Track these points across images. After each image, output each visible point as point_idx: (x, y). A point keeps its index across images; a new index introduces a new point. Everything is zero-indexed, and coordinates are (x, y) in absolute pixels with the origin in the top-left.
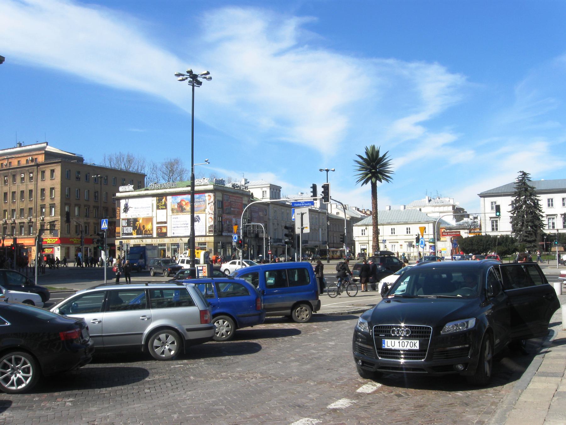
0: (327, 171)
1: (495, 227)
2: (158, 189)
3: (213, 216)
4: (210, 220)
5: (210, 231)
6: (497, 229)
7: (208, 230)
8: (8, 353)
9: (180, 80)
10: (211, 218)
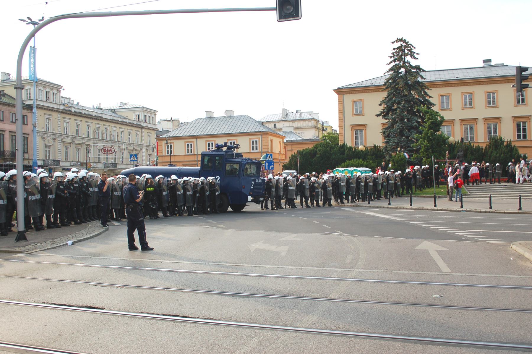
6: (525, 136)
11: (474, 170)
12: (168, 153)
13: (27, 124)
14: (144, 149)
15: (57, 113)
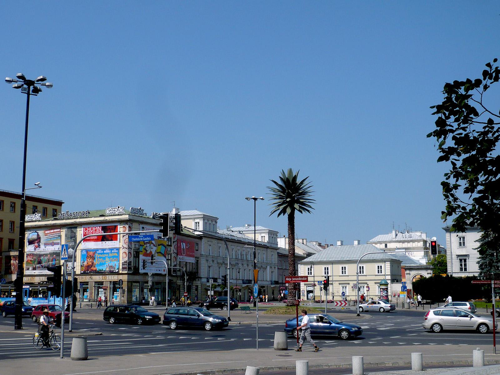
0: (255, 199)
1: (463, 268)
2: (68, 219)
3: (127, 251)
4: (125, 255)
5: (123, 268)
6: (466, 269)
7: (121, 267)
8: (252, 348)
9: (15, 87)
10: (125, 253)
11: (126, 312)
12: (325, 274)
13: (198, 250)
14: (268, 267)
15: (215, 240)
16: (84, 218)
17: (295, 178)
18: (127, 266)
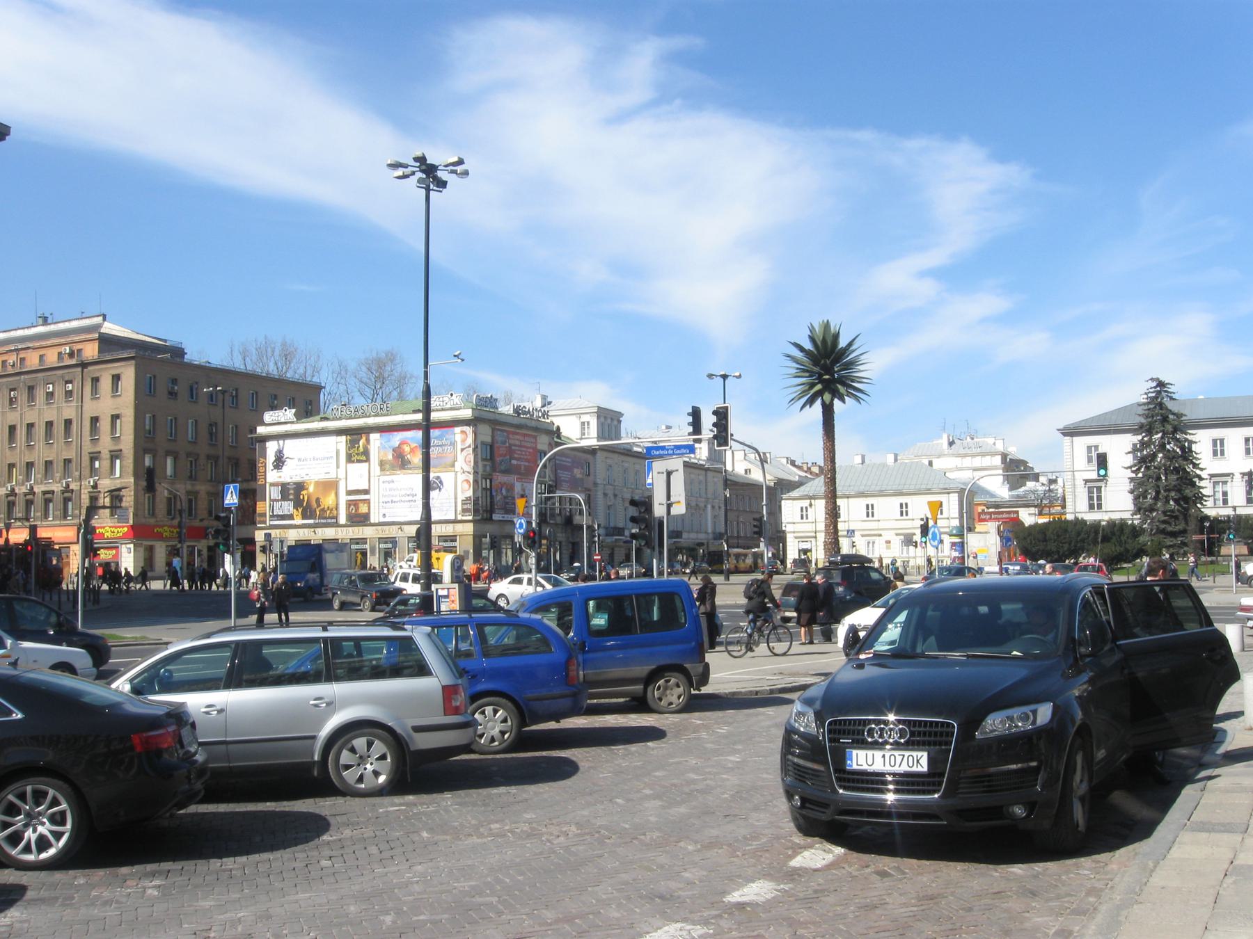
0: (725, 377)
1: (1095, 502)
3: (471, 478)
4: (466, 486)
5: (464, 511)
6: (1100, 506)
7: (459, 509)
9: (399, 178)
10: (467, 481)
16: (382, 415)
17: (836, 337)
18: (470, 506)
